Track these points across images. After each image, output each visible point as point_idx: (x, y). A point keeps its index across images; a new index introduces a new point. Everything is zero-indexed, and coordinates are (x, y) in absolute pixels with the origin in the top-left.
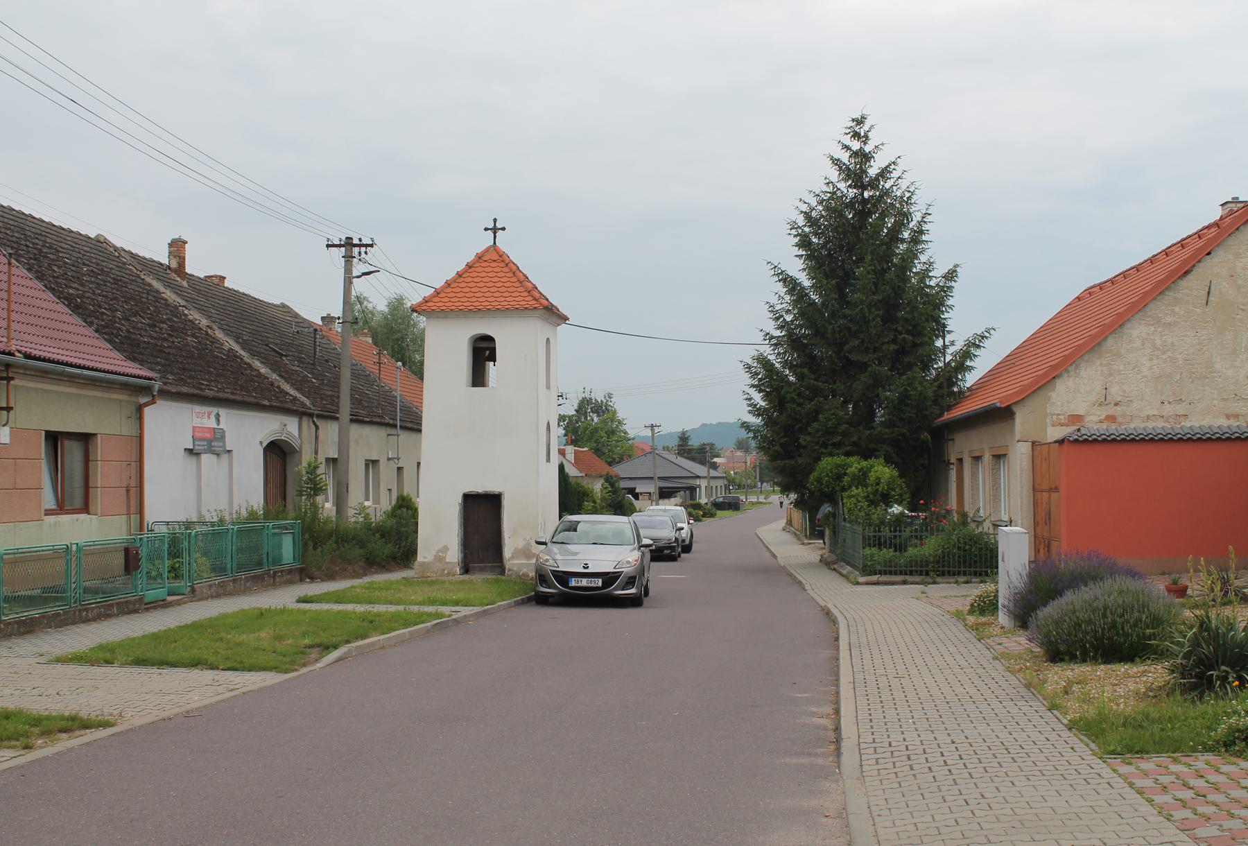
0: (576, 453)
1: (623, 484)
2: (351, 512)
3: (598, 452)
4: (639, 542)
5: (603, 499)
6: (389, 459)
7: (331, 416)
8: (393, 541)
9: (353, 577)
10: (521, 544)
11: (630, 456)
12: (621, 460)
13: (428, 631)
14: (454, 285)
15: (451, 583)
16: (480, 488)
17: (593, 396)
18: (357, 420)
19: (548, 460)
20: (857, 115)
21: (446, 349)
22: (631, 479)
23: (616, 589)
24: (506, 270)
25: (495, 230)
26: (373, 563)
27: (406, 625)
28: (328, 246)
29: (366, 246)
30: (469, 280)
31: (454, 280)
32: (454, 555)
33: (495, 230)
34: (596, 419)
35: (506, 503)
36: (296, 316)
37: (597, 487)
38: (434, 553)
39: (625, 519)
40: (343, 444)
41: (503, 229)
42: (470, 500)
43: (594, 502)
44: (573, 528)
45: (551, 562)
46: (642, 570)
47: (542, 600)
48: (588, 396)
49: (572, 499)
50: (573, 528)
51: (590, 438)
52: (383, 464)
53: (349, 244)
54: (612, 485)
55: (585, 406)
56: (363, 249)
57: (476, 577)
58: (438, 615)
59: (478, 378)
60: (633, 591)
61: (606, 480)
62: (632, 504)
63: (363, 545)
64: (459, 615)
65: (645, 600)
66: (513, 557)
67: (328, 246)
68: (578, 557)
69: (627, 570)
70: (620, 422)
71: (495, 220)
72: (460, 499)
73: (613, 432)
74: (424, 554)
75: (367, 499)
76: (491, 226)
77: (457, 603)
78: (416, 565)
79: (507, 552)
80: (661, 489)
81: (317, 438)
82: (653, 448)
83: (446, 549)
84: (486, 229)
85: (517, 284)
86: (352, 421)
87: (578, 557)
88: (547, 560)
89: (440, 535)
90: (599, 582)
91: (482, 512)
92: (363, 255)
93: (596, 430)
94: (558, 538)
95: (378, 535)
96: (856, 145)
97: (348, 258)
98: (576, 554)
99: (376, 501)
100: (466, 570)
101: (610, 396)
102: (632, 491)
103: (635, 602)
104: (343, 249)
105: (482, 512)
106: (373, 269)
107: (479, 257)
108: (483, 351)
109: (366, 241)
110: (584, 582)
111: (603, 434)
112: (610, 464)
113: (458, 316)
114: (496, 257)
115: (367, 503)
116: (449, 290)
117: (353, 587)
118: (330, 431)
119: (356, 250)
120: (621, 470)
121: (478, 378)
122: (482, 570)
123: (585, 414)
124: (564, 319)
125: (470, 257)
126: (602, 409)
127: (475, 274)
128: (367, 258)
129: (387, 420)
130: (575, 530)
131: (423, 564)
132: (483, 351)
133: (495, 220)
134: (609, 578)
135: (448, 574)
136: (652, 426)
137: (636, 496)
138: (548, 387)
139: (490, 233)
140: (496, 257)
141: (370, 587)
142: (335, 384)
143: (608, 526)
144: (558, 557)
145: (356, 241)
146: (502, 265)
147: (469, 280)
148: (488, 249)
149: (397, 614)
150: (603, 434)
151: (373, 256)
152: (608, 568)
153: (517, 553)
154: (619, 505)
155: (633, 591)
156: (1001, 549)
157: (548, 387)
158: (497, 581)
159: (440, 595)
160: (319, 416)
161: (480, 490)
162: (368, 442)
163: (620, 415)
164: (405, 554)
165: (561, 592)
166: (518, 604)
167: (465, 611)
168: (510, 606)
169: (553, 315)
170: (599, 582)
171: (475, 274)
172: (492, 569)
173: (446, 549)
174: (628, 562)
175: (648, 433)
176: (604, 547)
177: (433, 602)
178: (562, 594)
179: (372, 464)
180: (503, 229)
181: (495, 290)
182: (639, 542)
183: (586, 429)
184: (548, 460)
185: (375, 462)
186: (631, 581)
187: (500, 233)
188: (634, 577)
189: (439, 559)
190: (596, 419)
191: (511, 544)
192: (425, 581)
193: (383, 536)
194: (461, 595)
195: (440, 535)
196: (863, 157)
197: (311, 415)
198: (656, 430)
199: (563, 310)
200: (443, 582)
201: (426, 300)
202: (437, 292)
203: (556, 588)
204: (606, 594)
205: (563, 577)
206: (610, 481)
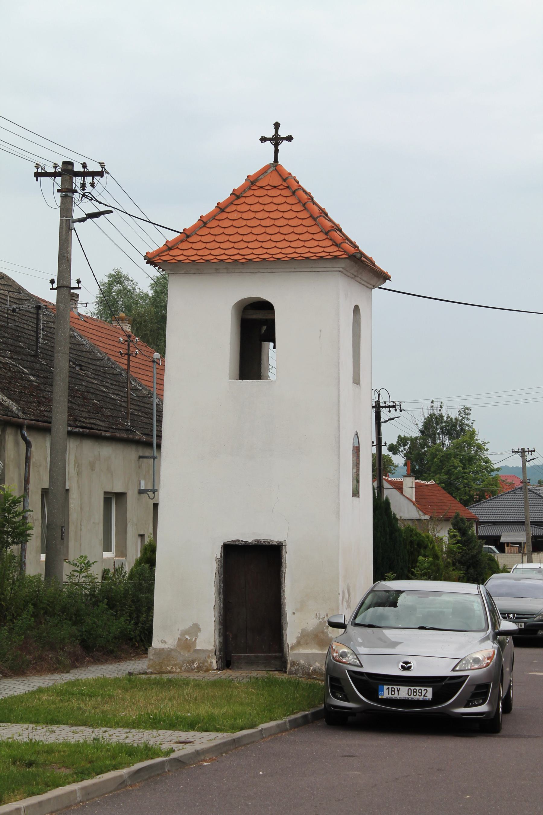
0: (418, 487)
1: (485, 531)
2: (67, 569)
3: (449, 487)
4: (495, 624)
5: (450, 552)
6: (141, 492)
7: (43, 428)
8: (121, 616)
9: (53, 670)
10: (311, 623)
11: (493, 493)
12: (481, 498)
13: (122, 783)
15: (198, 685)
16: (248, 535)
17: (444, 412)
18: (84, 432)
19: (356, 493)
21: (200, 324)
22: (494, 523)
23: (457, 704)
24: (291, 200)
25: (276, 140)
26: (93, 648)
27: (83, 774)
28: (38, 175)
29: (93, 174)
30: (235, 215)
31: (213, 216)
32: (208, 639)
33: (276, 140)
34: (447, 442)
35: (290, 559)
36: (20, 290)
37: (443, 534)
39: (472, 588)
40: (57, 470)
43: (436, 557)
44: (391, 600)
45: (351, 658)
46: (498, 671)
47: (337, 721)
48: (437, 412)
49: (397, 552)
50: (391, 600)
51: (439, 469)
52: (131, 499)
53: (67, 171)
54: (463, 532)
55: (432, 425)
56: (88, 179)
57: (238, 675)
58: (148, 752)
59: (250, 365)
60: (484, 708)
61: (455, 526)
62: (492, 560)
63: (77, 618)
64: (189, 749)
65: (507, 723)
67: (38, 175)
68: (398, 650)
69: (473, 673)
70: (480, 448)
71: (277, 126)
72: (218, 552)
73: (471, 460)
74: (163, 638)
75: (107, 548)
77: (191, 725)
78: (151, 651)
79: (290, 636)
80: (535, 537)
81: (28, 459)
82: (525, 482)
83: (196, 629)
84: (263, 140)
85: (309, 222)
86: (70, 434)
87: (398, 650)
88: (344, 655)
89: (187, 608)
90: (428, 693)
91: (252, 572)
92: (89, 188)
93: (447, 456)
94: (369, 615)
95: (103, 606)
97: (67, 192)
98: (395, 644)
99: (122, 552)
100: (227, 661)
101: (466, 411)
102: (495, 540)
103: (487, 726)
104: (59, 180)
105: (252, 572)
106: (103, 208)
107: (252, 182)
108: (256, 327)
109: (93, 167)
110: (403, 693)
111: (457, 462)
112: (466, 503)
114: (277, 181)
115: (94, 555)
116: (205, 231)
117: (40, 691)
118: (42, 449)
119: (78, 180)
120: (481, 511)
121: (250, 365)
122: (251, 663)
123: (434, 437)
124: (384, 277)
125: (239, 182)
126: (456, 428)
127: (244, 208)
128: (94, 193)
129: (138, 435)
130: (394, 604)
131: (160, 652)
132: (256, 327)
133: (277, 126)
134: (444, 686)
135: (199, 669)
136: (523, 452)
137: (502, 548)
138: (356, 381)
139: (269, 146)
140: (277, 181)
141: (63, 693)
142: (47, 377)
143: (445, 598)
144: (361, 650)
145: (78, 168)
146: (286, 193)
147: (235, 215)
148: (264, 171)
149: (77, 749)
150: (457, 462)
151: (103, 189)
152: (442, 669)
153: (305, 638)
154: (473, 566)
155: (484, 708)
157: (356, 381)
158: (270, 683)
159: (169, 707)
160: (30, 428)
161: (250, 539)
162: (94, 469)
163: (480, 438)
164: (138, 638)
165: (363, 707)
166: (296, 725)
167: (202, 740)
168: (281, 729)
169: (366, 271)
170: (428, 693)
171: (244, 208)
172: (267, 663)
173: (196, 629)
174: (476, 661)
175: (516, 462)
176: (439, 638)
177: (156, 723)
178: (367, 710)
179: (114, 499)
180: (289, 138)
181: (274, 234)
182: (495, 624)
183: (434, 456)
184: (356, 493)
185: (120, 496)
186: (480, 692)
187: (284, 146)
188: (486, 686)
189: (186, 644)
190: (447, 442)
191: (296, 624)
192: (162, 682)
193: (111, 606)
194: (204, 710)
195: (187, 608)
197: (19, 427)
198: (529, 456)
199: (381, 264)
200: (186, 683)
201: (169, 247)
202: (186, 235)
203: (357, 700)
204: (438, 712)
205: (370, 683)
206: (460, 526)
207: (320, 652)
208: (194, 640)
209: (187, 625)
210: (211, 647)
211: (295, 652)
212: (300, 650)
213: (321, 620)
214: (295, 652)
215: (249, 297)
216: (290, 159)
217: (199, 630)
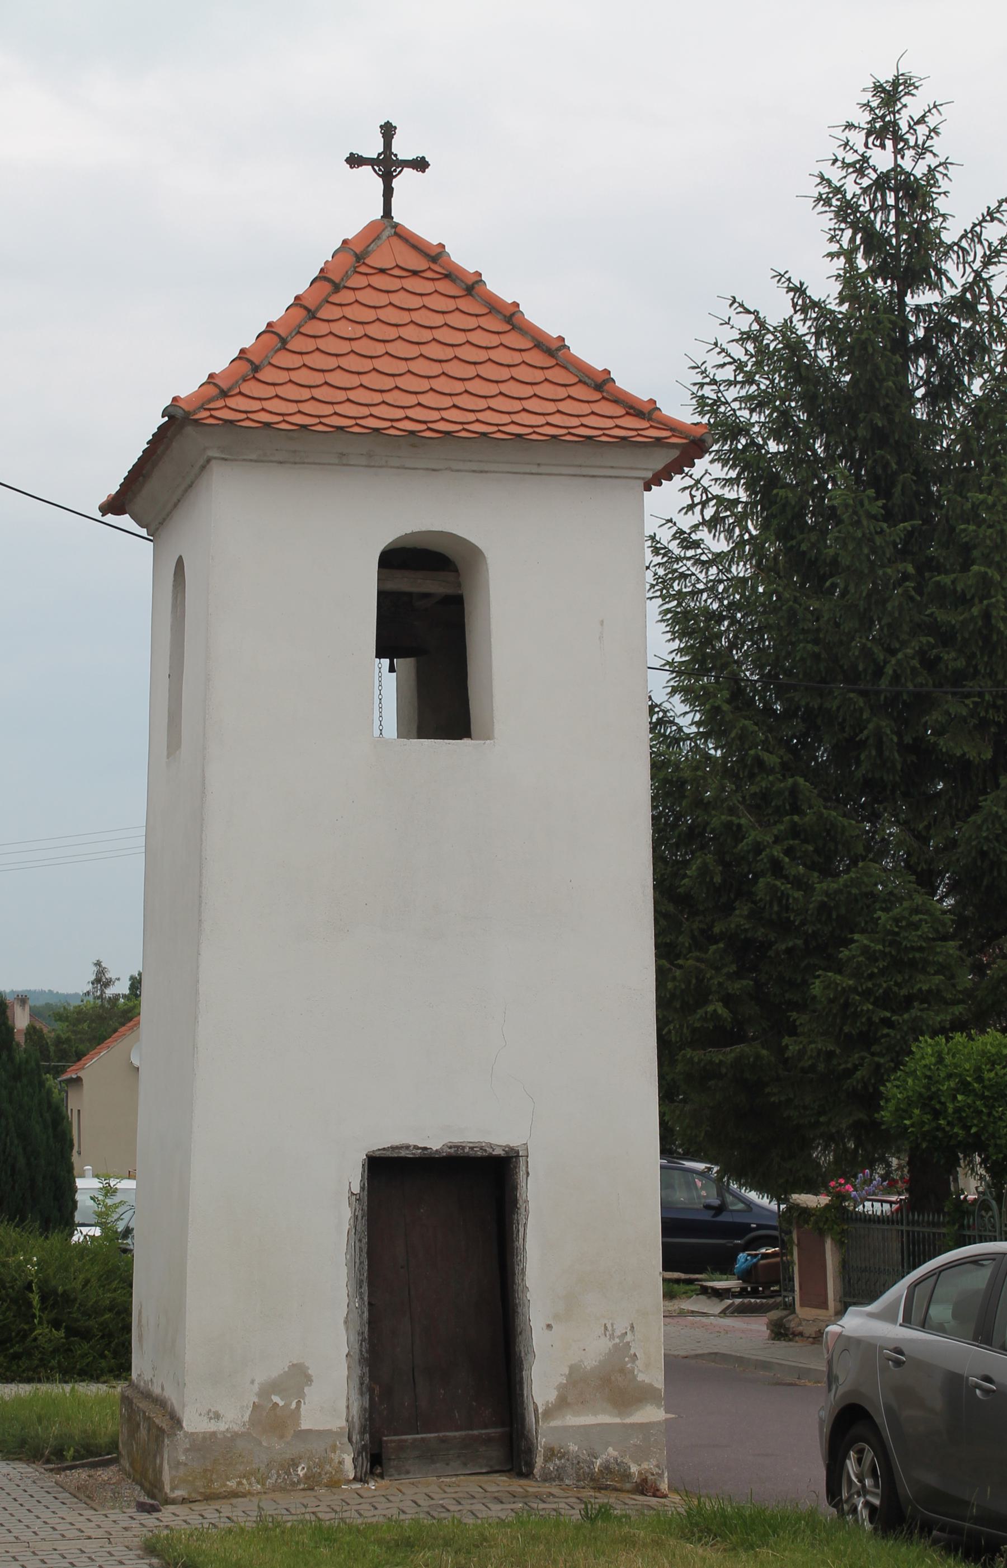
10: (593, 1349)
14: (297, 343)
16: (431, 1132)
20: (886, 76)
25: (387, 166)
31: (452, 274)
32: (331, 1402)
33: (387, 166)
35: (537, 1194)
38: (252, 1398)
41: (420, 164)
42: (390, 1175)
66: (562, 1403)
72: (354, 1178)
76: (373, 148)
79: (542, 1383)
83: (299, 1377)
96: (883, 159)
100: (375, 1460)
113: (343, 461)
122: (430, 1457)
133: (388, 131)
135: (311, 1482)
139: (369, 179)
153: (578, 1389)
156: (952, 1370)
173: (299, 1377)
187: (405, 180)
189: (273, 1418)
196: (915, 193)
207: (618, 1420)
208: (294, 1405)
209: (276, 1368)
210: (337, 1422)
211: (553, 1424)
212: (568, 1418)
213: (617, 1340)
214: (553, 1424)
215: (424, 529)
216: (422, 209)
217: (308, 1380)
